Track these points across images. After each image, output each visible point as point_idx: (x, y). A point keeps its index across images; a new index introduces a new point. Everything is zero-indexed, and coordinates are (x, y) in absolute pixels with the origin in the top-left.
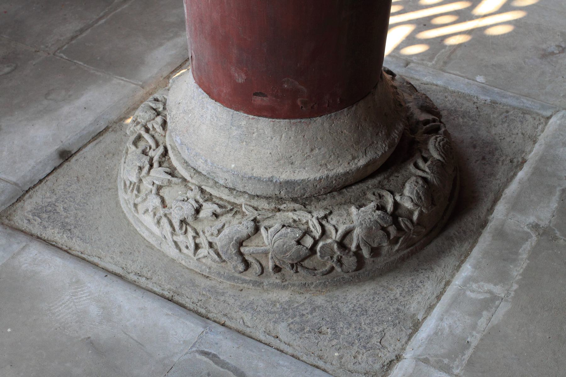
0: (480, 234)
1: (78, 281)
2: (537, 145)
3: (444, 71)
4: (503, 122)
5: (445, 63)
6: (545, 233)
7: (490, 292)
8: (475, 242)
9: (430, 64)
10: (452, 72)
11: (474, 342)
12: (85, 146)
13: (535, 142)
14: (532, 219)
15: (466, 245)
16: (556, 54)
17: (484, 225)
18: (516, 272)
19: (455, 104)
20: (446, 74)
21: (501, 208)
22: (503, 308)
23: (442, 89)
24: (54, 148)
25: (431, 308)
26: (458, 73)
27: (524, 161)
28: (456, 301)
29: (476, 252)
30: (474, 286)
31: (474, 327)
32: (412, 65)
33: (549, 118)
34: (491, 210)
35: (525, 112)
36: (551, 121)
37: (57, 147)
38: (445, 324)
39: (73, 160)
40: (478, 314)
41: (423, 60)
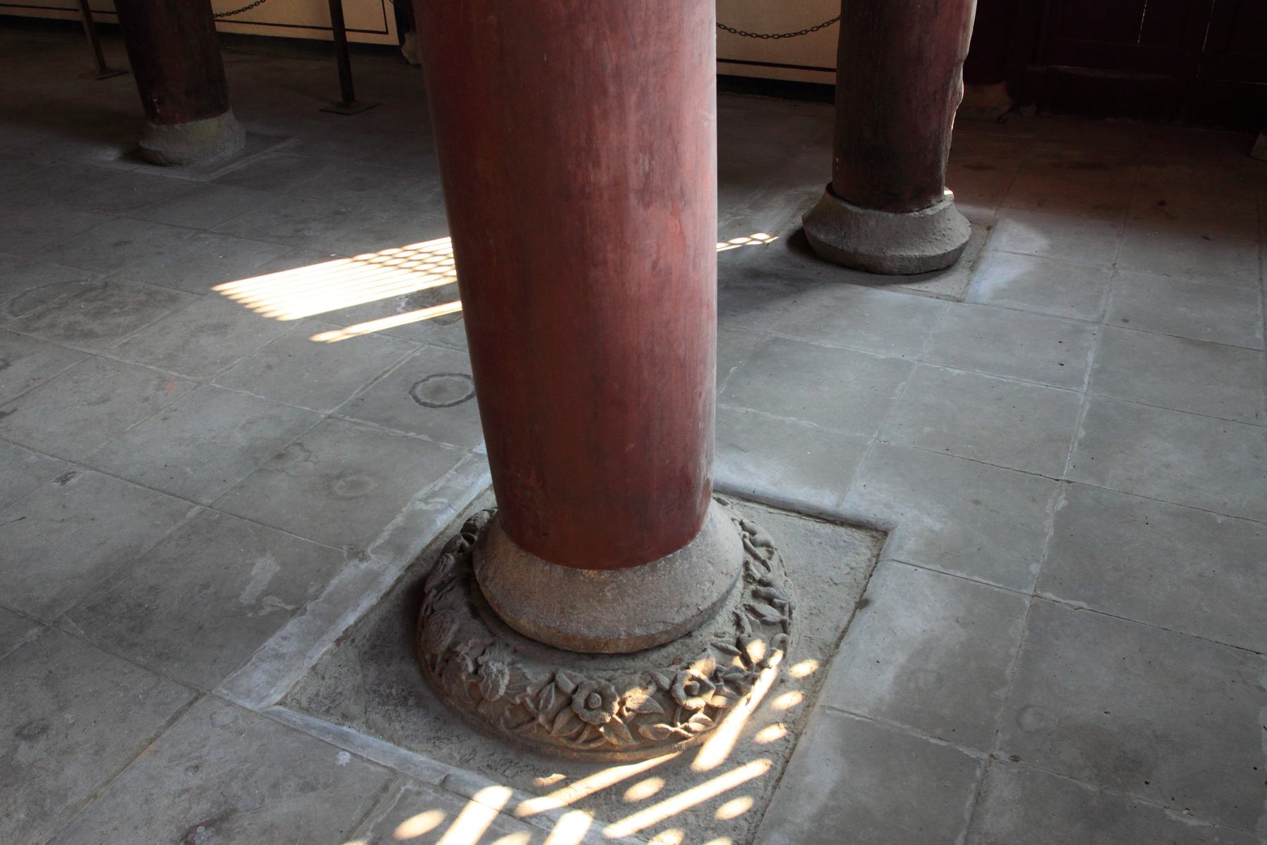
0: (417, 559)
1: (775, 485)
2: (314, 662)
3: (392, 770)
4: (341, 693)
5: (385, 789)
6: (358, 554)
7: (427, 503)
8: (424, 551)
9: (409, 786)
10: (381, 770)
11: (452, 471)
12: (849, 622)
13: (314, 668)
14: (364, 566)
15: (434, 547)
16: (201, 824)
17: (410, 567)
18: (399, 520)
19: (393, 715)
20: (390, 764)
21: (389, 579)
22: (421, 494)
23: (405, 743)
24: (878, 604)
25: (478, 498)
26: (372, 768)
27: (338, 641)
28: (458, 496)
29: (428, 539)
30: (439, 506)
31: (449, 480)
32: (437, 781)
33: (280, 703)
34: (399, 580)
35: (307, 711)
36: (279, 697)
37: (876, 605)
38: (471, 480)
39: (852, 605)
40: (442, 488)
41: (418, 793)
